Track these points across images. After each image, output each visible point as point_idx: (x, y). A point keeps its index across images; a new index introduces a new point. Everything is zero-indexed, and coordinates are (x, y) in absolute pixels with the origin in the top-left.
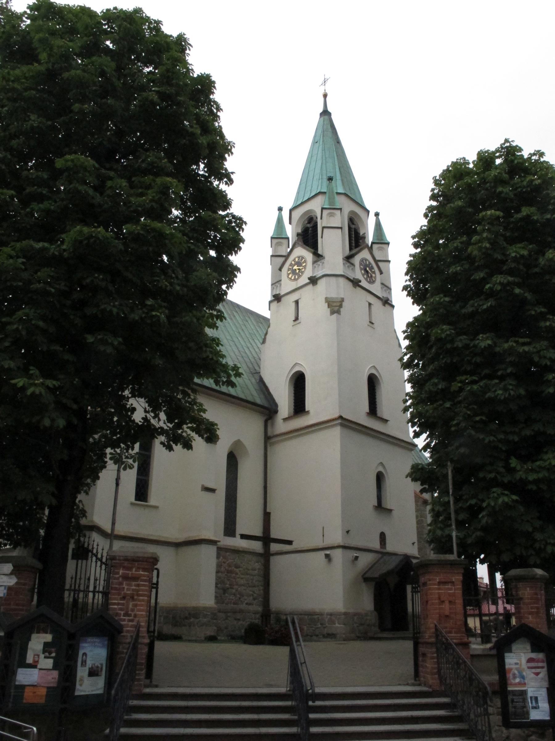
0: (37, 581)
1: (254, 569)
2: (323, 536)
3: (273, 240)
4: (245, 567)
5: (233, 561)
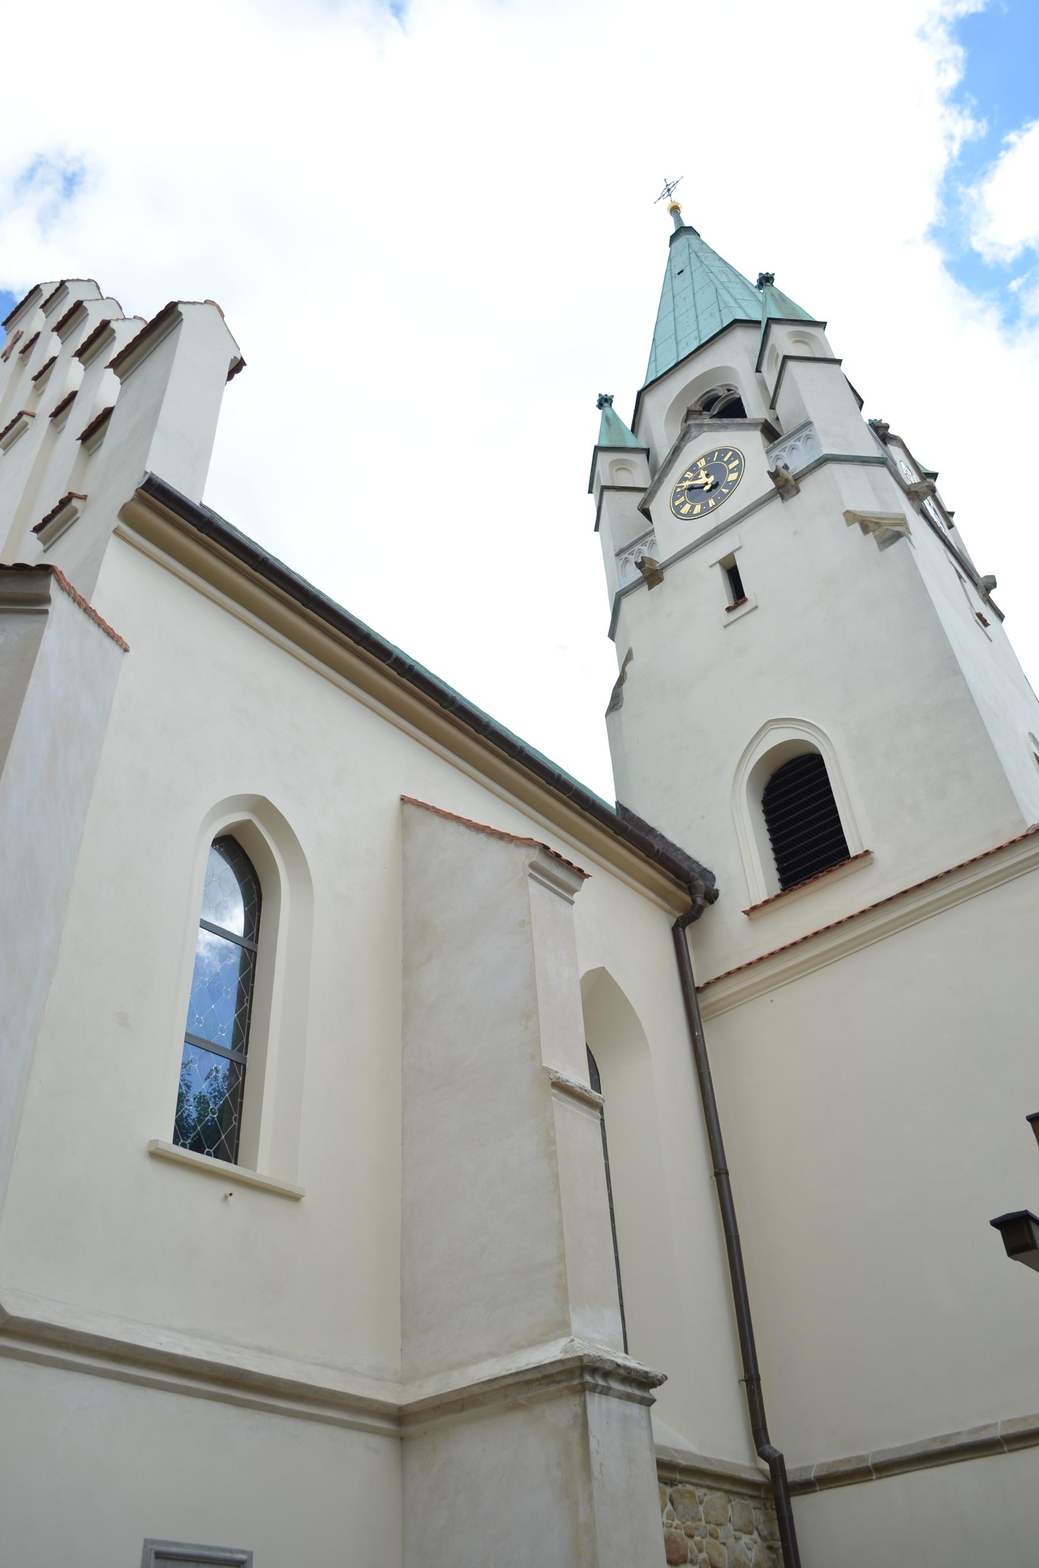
3: (601, 455)
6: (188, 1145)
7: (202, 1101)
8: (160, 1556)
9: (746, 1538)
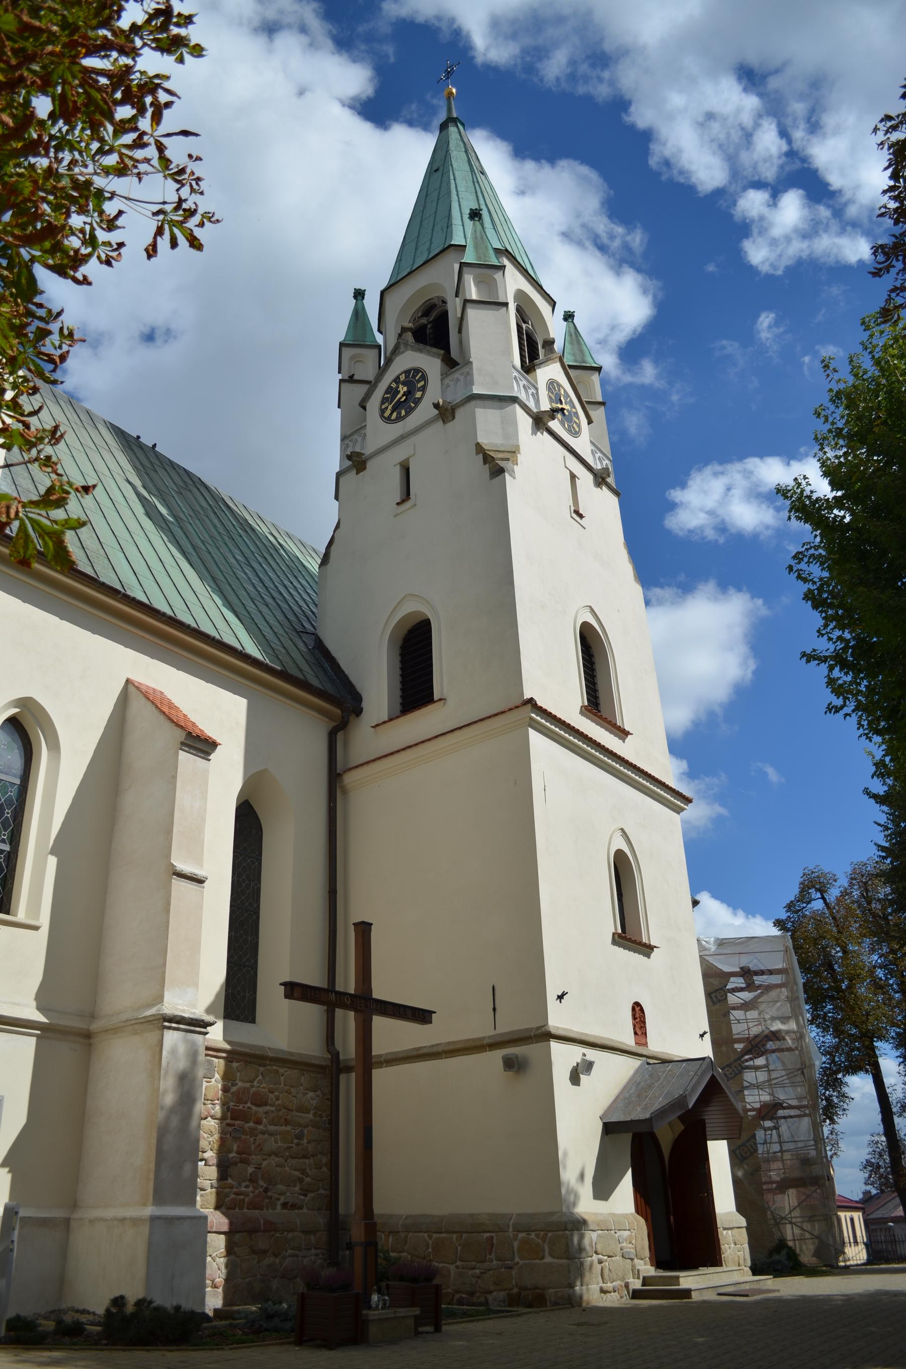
0: (883, 1266)
1: (303, 1109)
2: (494, 1009)
3: (344, 349)
4: (279, 1102)
5: (248, 1085)
6: (548, 1304)
7: (54, 441)
9: (311, 1094)
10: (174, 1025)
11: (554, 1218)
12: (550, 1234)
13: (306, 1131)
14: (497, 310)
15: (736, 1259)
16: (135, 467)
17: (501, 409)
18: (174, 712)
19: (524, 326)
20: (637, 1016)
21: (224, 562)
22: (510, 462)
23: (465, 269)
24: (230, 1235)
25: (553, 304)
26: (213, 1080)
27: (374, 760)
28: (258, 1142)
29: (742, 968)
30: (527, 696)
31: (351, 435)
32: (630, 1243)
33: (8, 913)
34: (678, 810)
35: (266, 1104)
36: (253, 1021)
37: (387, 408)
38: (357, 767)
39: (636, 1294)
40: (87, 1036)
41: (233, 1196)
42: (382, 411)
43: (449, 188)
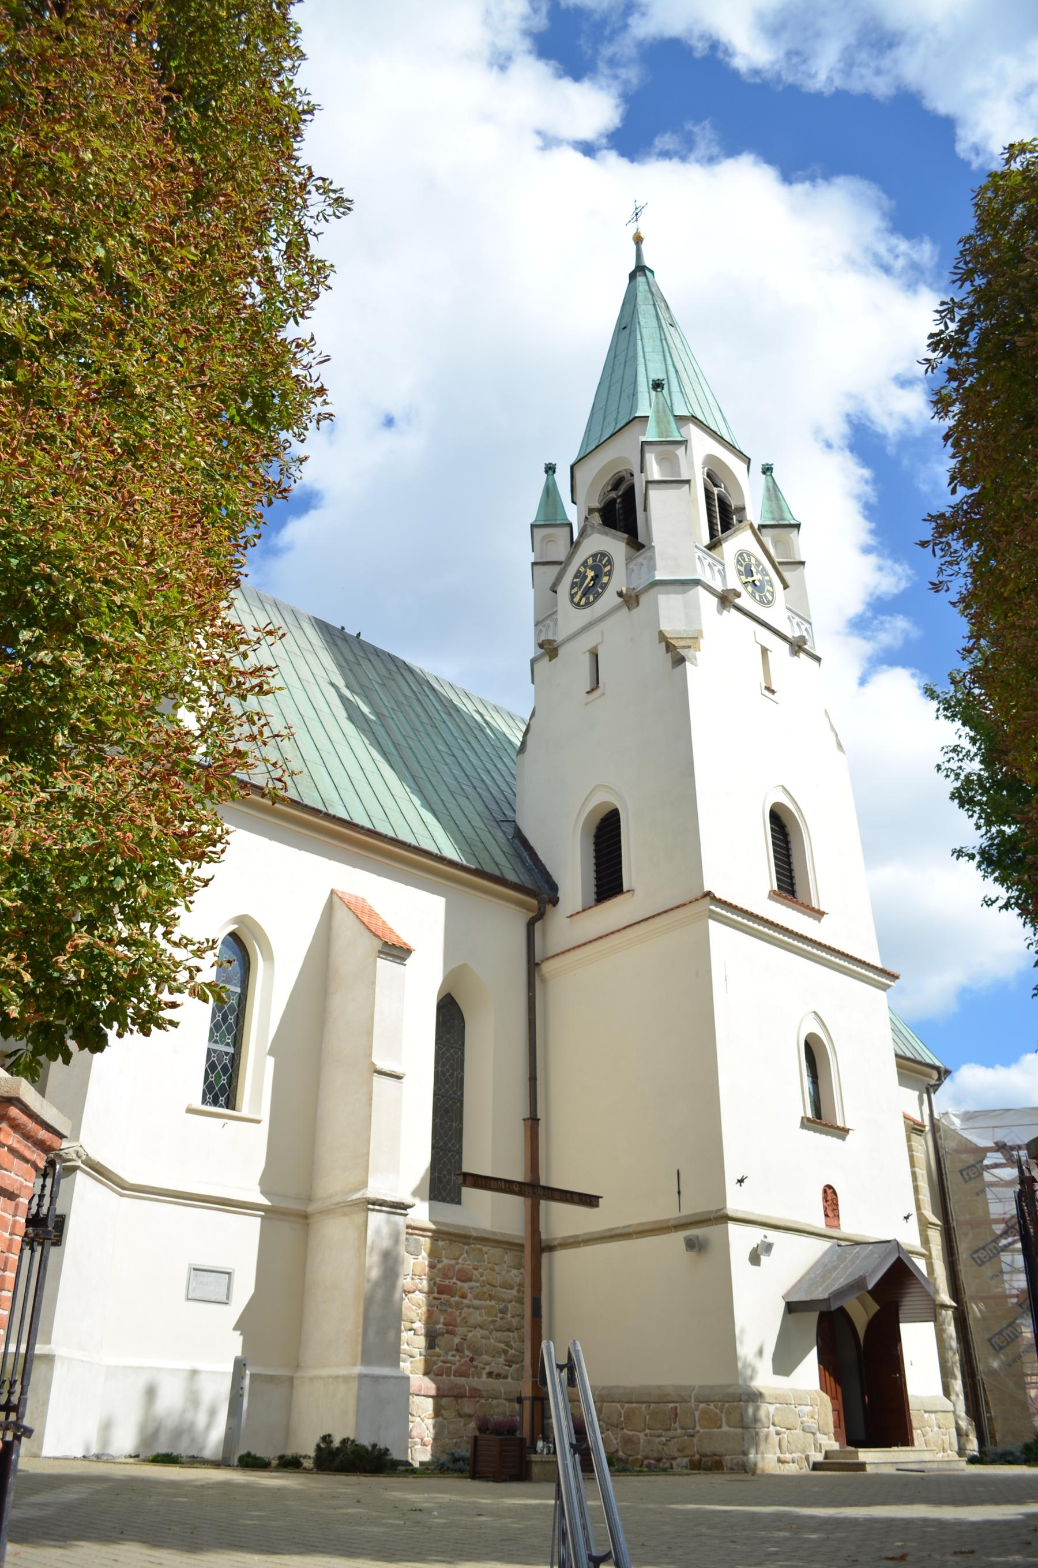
2: (679, 1192)
3: (535, 530)
4: (484, 1278)
5: (453, 1262)
8: (195, 1269)
9: (514, 1272)
10: (377, 1207)
11: (731, 1390)
12: (727, 1405)
13: (510, 1306)
14: (680, 488)
15: (940, 1442)
16: (339, 666)
17: (684, 593)
18: (373, 921)
19: (716, 490)
20: (829, 1198)
21: (426, 756)
22: (692, 650)
23: (647, 448)
24: (437, 1398)
25: (748, 461)
26: (420, 1257)
27: (569, 950)
28: (463, 1315)
29: (996, 1143)
30: (706, 889)
31: (543, 620)
32: (812, 1417)
33: (234, 1109)
34: (884, 988)
35: (470, 1280)
36: (459, 1202)
37: (576, 593)
38: (553, 957)
39: (816, 1466)
40: (305, 1216)
41: (440, 1364)
42: (572, 596)
43: (636, 349)
